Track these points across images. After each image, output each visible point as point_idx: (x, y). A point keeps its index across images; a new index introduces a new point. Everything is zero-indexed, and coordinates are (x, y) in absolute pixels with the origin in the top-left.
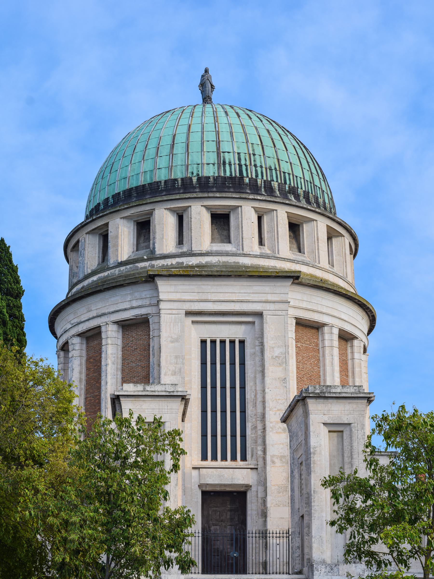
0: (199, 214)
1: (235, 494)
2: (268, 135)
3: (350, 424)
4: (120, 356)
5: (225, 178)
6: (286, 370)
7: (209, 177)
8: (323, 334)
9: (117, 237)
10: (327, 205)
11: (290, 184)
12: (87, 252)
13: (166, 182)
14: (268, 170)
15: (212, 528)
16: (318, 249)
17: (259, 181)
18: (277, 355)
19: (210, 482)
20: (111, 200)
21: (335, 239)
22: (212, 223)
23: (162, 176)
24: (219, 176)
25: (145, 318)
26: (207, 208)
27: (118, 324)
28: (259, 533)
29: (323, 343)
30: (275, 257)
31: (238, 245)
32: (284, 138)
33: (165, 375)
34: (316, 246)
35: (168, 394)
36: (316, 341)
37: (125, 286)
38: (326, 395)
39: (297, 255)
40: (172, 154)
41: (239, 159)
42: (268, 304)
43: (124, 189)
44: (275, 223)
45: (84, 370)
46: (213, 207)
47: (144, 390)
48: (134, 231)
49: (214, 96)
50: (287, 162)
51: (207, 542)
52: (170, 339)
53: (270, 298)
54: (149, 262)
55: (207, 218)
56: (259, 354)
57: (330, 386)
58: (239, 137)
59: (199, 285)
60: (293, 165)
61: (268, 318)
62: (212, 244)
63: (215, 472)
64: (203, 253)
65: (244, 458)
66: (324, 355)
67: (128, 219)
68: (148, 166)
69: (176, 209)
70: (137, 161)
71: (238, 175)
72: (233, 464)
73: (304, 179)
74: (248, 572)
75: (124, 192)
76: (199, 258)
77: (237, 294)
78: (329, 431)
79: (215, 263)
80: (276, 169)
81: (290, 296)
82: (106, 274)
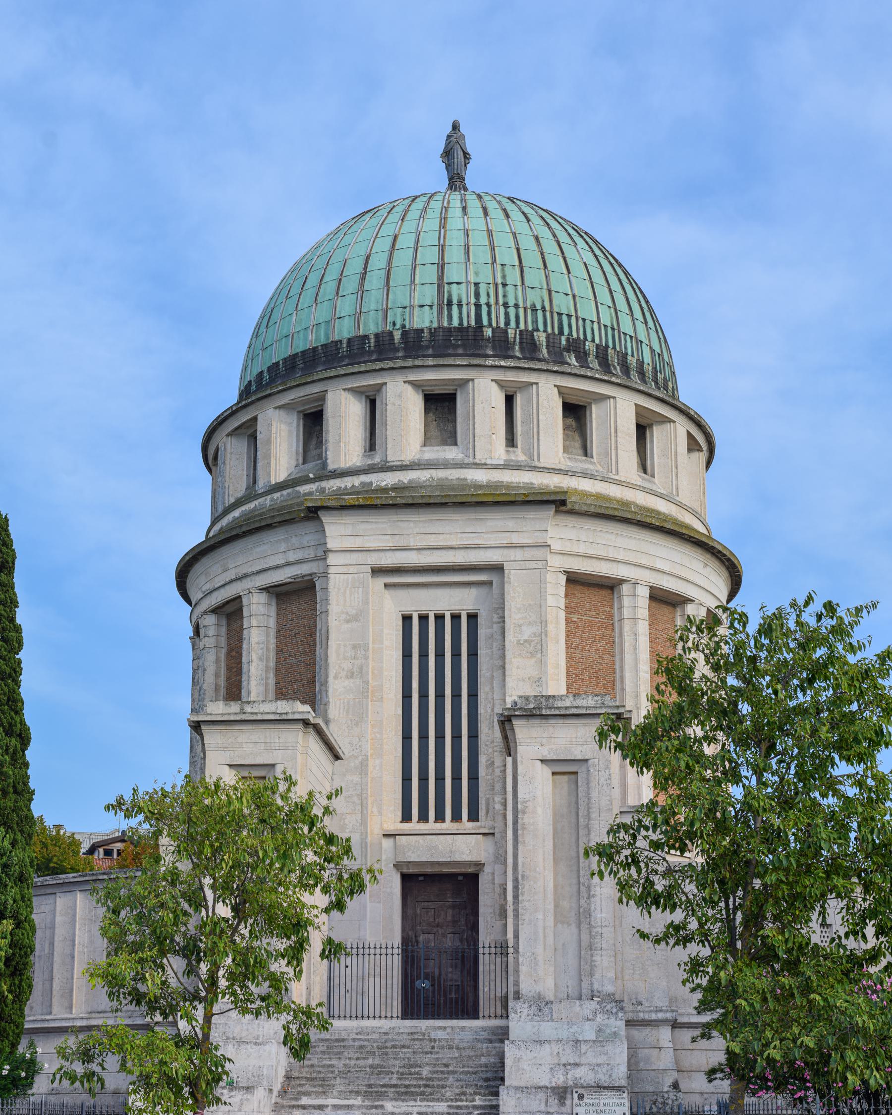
0: (400, 396)
1: (460, 878)
2: (535, 247)
3: (586, 760)
4: (272, 646)
6: (542, 664)
7: (422, 330)
9: (269, 442)
10: (648, 369)
11: (570, 334)
12: (228, 467)
13: (349, 340)
14: (529, 311)
15: (422, 938)
17: (511, 333)
19: (413, 858)
20: (266, 376)
21: (659, 427)
22: (427, 410)
23: (344, 331)
24: (439, 327)
25: (309, 580)
26: (415, 385)
27: (269, 592)
28: (496, 947)
29: (621, 613)
30: (531, 467)
31: (468, 449)
32: (569, 251)
33: (336, 677)
34: (613, 442)
35: (278, 718)
36: (608, 609)
37: (276, 527)
38: (544, 712)
39: (576, 460)
40: (361, 290)
41: (477, 295)
42: (512, 551)
43: (286, 356)
45: (223, 671)
48: (298, 430)
49: (472, 176)
50: (567, 295)
51: (413, 961)
52: (344, 616)
53: (516, 539)
54: (317, 484)
55: (414, 404)
56: (499, 637)
57: (554, 696)
58: (481, 254)
59: (394, 522)
60: (578, 299)
61: (512, 575)
63: (421, 841)
64: (406, 466)
65: (474, 817)
68: (322, 313)
69: (362, 389)
70: (306, 305)
71: (473, 323)
72: (440, 827)
73: (599, 322)
74: (481, 1014)
75: (285, 360)
76: (399, 473)
77: (460, 535)
78: (553, 774)
79: (424, 482)
80: (543, 309)
81: (550, 534)
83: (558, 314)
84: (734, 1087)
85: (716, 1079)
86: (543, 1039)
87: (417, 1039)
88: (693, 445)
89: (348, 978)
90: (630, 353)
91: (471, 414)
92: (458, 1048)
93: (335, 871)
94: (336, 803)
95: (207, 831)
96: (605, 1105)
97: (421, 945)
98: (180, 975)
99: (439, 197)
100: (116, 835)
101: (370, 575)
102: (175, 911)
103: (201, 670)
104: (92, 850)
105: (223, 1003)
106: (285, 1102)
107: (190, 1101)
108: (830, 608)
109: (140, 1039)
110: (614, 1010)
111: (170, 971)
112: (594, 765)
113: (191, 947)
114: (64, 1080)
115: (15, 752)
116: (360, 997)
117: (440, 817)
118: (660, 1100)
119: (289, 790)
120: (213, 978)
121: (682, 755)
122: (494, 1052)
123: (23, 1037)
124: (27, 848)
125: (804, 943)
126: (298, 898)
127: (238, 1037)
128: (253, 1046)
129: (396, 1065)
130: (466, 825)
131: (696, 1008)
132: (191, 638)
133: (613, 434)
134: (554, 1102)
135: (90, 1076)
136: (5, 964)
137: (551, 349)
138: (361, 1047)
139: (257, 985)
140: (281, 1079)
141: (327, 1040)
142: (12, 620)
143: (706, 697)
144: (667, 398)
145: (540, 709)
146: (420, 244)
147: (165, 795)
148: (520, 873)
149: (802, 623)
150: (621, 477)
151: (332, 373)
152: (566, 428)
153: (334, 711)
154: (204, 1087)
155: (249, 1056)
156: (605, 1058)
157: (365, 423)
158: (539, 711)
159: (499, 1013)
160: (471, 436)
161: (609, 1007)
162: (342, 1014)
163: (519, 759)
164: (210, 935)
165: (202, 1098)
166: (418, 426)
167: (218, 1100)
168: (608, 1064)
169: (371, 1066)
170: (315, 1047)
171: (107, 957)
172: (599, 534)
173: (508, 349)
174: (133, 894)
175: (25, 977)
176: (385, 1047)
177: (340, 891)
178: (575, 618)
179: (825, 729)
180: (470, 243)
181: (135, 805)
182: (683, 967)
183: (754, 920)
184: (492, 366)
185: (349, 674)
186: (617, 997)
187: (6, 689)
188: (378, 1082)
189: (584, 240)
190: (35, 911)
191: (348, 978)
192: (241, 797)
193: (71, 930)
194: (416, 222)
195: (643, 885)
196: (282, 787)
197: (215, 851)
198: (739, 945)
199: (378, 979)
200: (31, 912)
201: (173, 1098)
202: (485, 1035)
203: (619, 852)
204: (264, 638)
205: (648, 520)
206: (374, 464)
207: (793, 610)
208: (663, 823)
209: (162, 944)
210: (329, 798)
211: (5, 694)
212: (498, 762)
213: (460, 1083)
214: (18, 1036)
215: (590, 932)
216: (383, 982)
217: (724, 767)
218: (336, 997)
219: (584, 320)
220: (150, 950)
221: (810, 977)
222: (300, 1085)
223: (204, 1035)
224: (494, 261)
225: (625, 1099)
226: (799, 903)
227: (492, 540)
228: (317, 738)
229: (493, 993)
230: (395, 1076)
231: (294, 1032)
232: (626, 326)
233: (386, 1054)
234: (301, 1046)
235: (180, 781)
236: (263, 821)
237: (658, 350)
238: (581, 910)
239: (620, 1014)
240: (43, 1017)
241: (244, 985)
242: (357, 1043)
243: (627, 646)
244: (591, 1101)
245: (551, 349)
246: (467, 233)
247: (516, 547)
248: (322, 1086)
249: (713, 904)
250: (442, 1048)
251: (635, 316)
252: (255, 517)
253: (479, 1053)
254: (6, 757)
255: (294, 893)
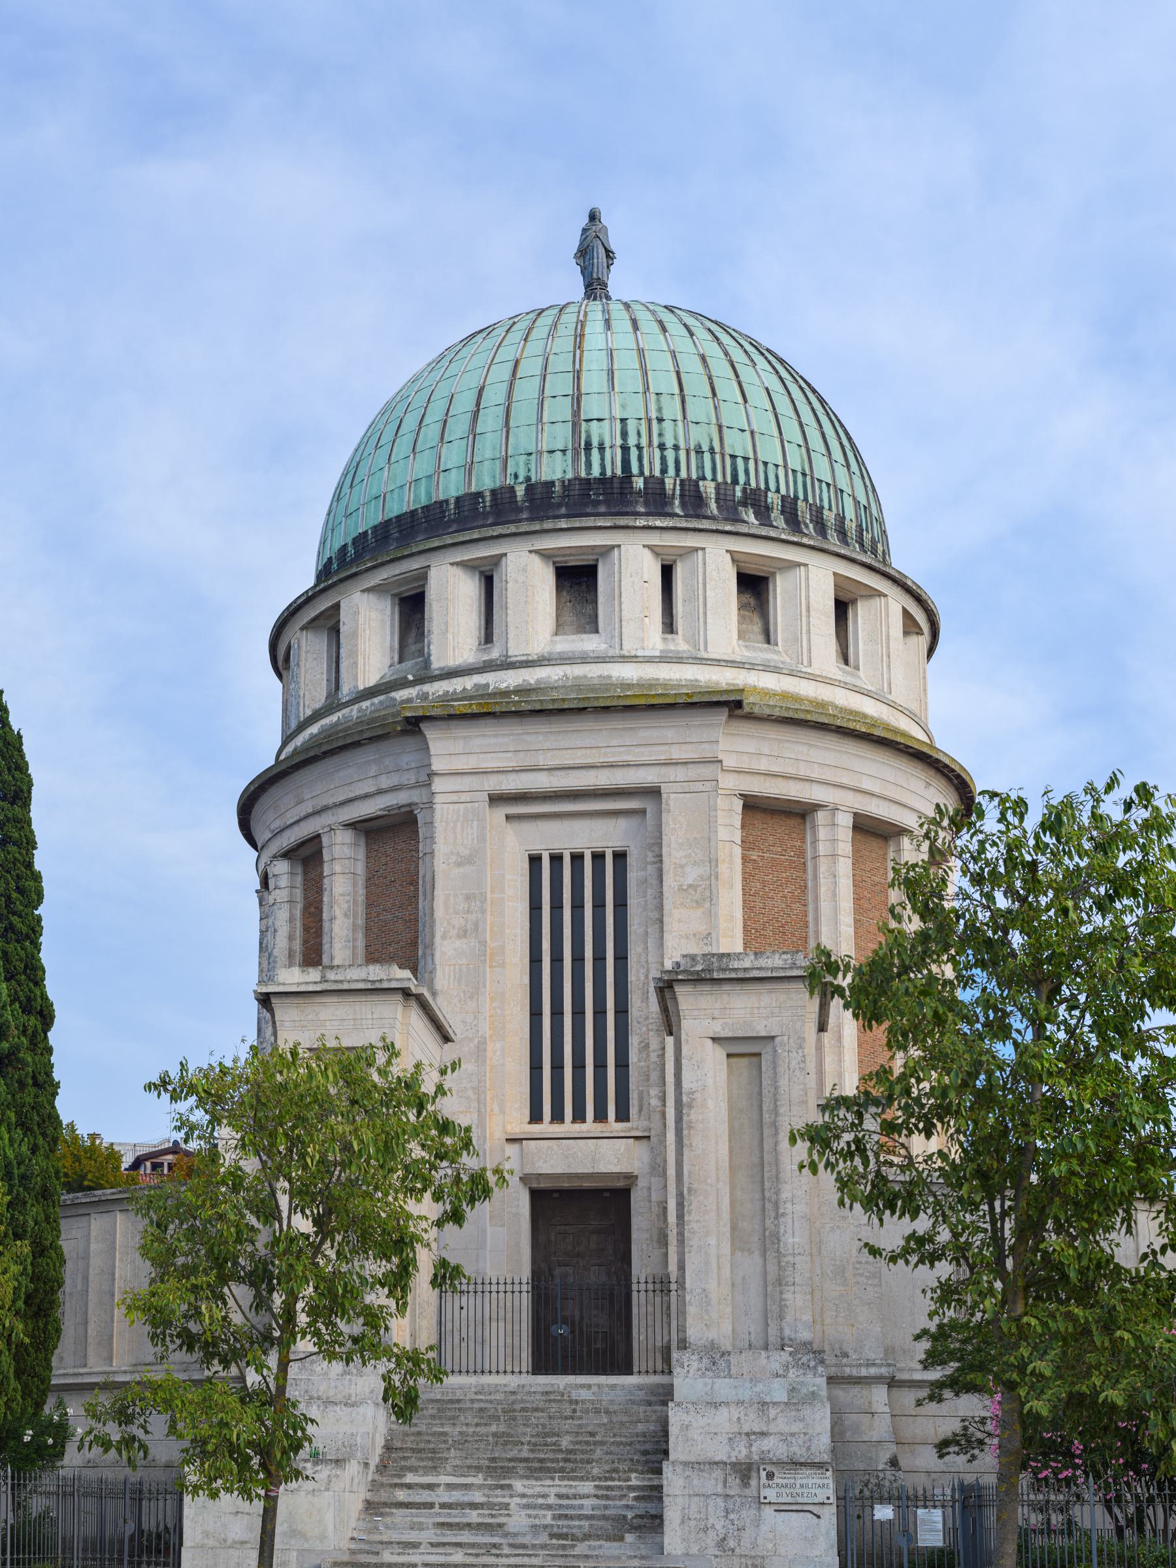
0: (524, 570)
1: (607, 1194)
3: (773, 1038)
4: (361, 898)
5: (587, 483)
6: (711, 915)
7: (552, 483)
8: (814, 827)
9: (355, 635)
10: (851, 526)
11: (747, 482)
12: (303, 670)
13: (458, 499)
14: (693, 454)
15: (557, 1271)
16: (809, 632)
17: (669, 484)
18: (690, 882)
22: (559, 588)
23: (452, 487)
24: (576, 478)
26: (544, 554)
29: (815, 849)
30: (696, 658)
31: (613, 637)
32: (746, 373)
33: (444, 937)
34: (804, 624)
36: (798, 844)
38: (715, 975)
40: (473, 433)
41: (624, 434)
42: (671, 769)
43: (376, 523)
44: (700, 579)
45: (298, 932)
46: (556, 552)
47: (324, 980)
48: (393, 619)
49: (619, 283)
50: (743, 431)
52: (453, 858)
53: (677, 753)
54: (418, 688)
55: (543, 579)
57: (729, 955)
60: (757, 436)
61: (673, 800)
62: (558, 638)
64: (532, 661)
65: (623, 1115)
66: (816, 877)
67: (378, 591)
68: (423, 465)
69: (476, 563)
71: (619, 472)
72: (578, 1128)
73: (785, 466)
74: (636, 1369)
75: (375, 528)
77: (603, 750)
78: (729, 1056)
80: (712, 451)
81: (722, 746)
82: (334, 718)
83: (731, 456)
84: (1004, 1460)
85: (948, 1453)
86: (718, 1400)
87: (554, 1401)
88: (910, 626)
89: (464, 1323)
90: (826, 506)
91: (617, 591)
92: (607, 1412)
93: (449, 1171)
94: (450, 1081)
95: (281, 1116)
96: (802, 1486)
97: (557, 1280)
98: (247, 1311)
99: (572, 309)
100: (166, 1146)
101: (487, 804)
102: (237, 1226)
103: (271, 930)
104: (137, 1164)
105: (305, 1345)
106: (384, 1480)
107: (261, 1476)
108: (1144, 792)
109: (193, 1395)
110: (812, 1364)
111: (231, 1302)
112: (782, 1044)
113: (260, 1271)
114: (94, 1446)
115: (35, 1034)
116: (479, 1348)
117: (579, 1117)
118: (874, 1481)
119: (389, 1063)
120: (289, 1313)
121: (928, 1000)
122: (654, 1418)
123: (49, 1394)
124: (51, 1155)
125: (1104, 1260)
126: (401, 1207)
127: (324, 1397)
128: (344, 1408)
129: (527, 1433)
130: (614, 1126)
131: (921, 1362)
132: (257, 891)
133: (804, 613)
134: (734, 1481)
135: (128, 1441)
136: (25, 1303)
137: (722, 503)
138: (481, 1410)
139: (349, 1321)
140: (379, 1451)
141: (437, 1401)
142: (29, 865)
143: (962, 922)
144: (876, 565)
145: (710, 971)
146: (549, 371)
147: (224, 1071)
148: (686, 1185)
149: (1101, 816)
150: (815, 670)
151: (436, 543)
152: (742, 607)
153: (442, 979)
154: (279, 1455)
155: (338, 1421)
156: (801, 1425)
157: (480, 607)
158: (709, 974)
159: (659, 1367)
160: (617, 620)
161: (804, 1360)
162: (456, 1369)
163: (683, 1037)
164: (284, 1255)
165: (277, 1471)
166: (548, 609)
167: (297, 1474)
168: (805, 1434)
169: (495, 1435)
170: (422, 1409)
171: (150, 1284)
172: (786, 745)
173: (665, 504)
174: (183, 1204)
175: (51, 1319)
176: (512, 1409)
177: (456, 1196)
178: (754, 855)
179: (1137, 961)
180: (615, 367)
181: (184, 1085)
182: (929, 1294)
183: (1030, 1229)
184: (644, 528)
185: (461, 933)
186: (815, 1347)
187: (22, 953)
188: (504, 1455)
189: (766, 358)
190: (63, 1236)
191: (464, 1323)
192: (326, 1069)
193: (107, 1255)
194: (542, 342)
195: (873, 1181)
196: (381, 1058)
197: (294, 1142)
198: (1009, 1264)
199: (501, 1324)
200: (58, 1237)
201: (235, 1471)
202: (641, 1395)
203: (838, 1137)
204: (350, 888)
205: (851, 725)
206: (492, 661)
207: (1089, 797)
208: (901, 1094)
209: (223, 1269)
210: (443, 1072)
211: (21, 960)
212: (654, 1045)
213: (611, 1457)
214: (44, 1394)
215: (779, 1262)
216: (509, 1327)
217: (987, 1017)
218: (449, 1347)
219: (765, 464)
220: (207, 1275)
221: (1114, 1307)
222: (404, 1458)
223: (277, 1388)
224: (647, 389)
225: (829, 1479)
226: (1099, 1206)
227: (646, 755)
228: (421, 1013)
229: (651, 1341)
230: (526, 1447)
231: (398, 1384)
232: (822, 470)
233: (514, 1419)
234: (406, 1403)
235: (244, 1054)
236: (354, 1102)
237: (863, 501)
238: (767, 1233)
239: (820, 1369)
240: (76, 1371)
241: (331, 1323)
242: (476, 1405)
243: (823, 891)
244: (784, 1482)
245: (722, 503)
246: (611, 354)
247: (677, 764)
248: (432, 1459)
249: (974, 1207)
250: (587, 1411)
251: (834, 457)
252: (338, 733)
253: (635, 1419)
254: (23, 1039)
255: (396, 1199)
